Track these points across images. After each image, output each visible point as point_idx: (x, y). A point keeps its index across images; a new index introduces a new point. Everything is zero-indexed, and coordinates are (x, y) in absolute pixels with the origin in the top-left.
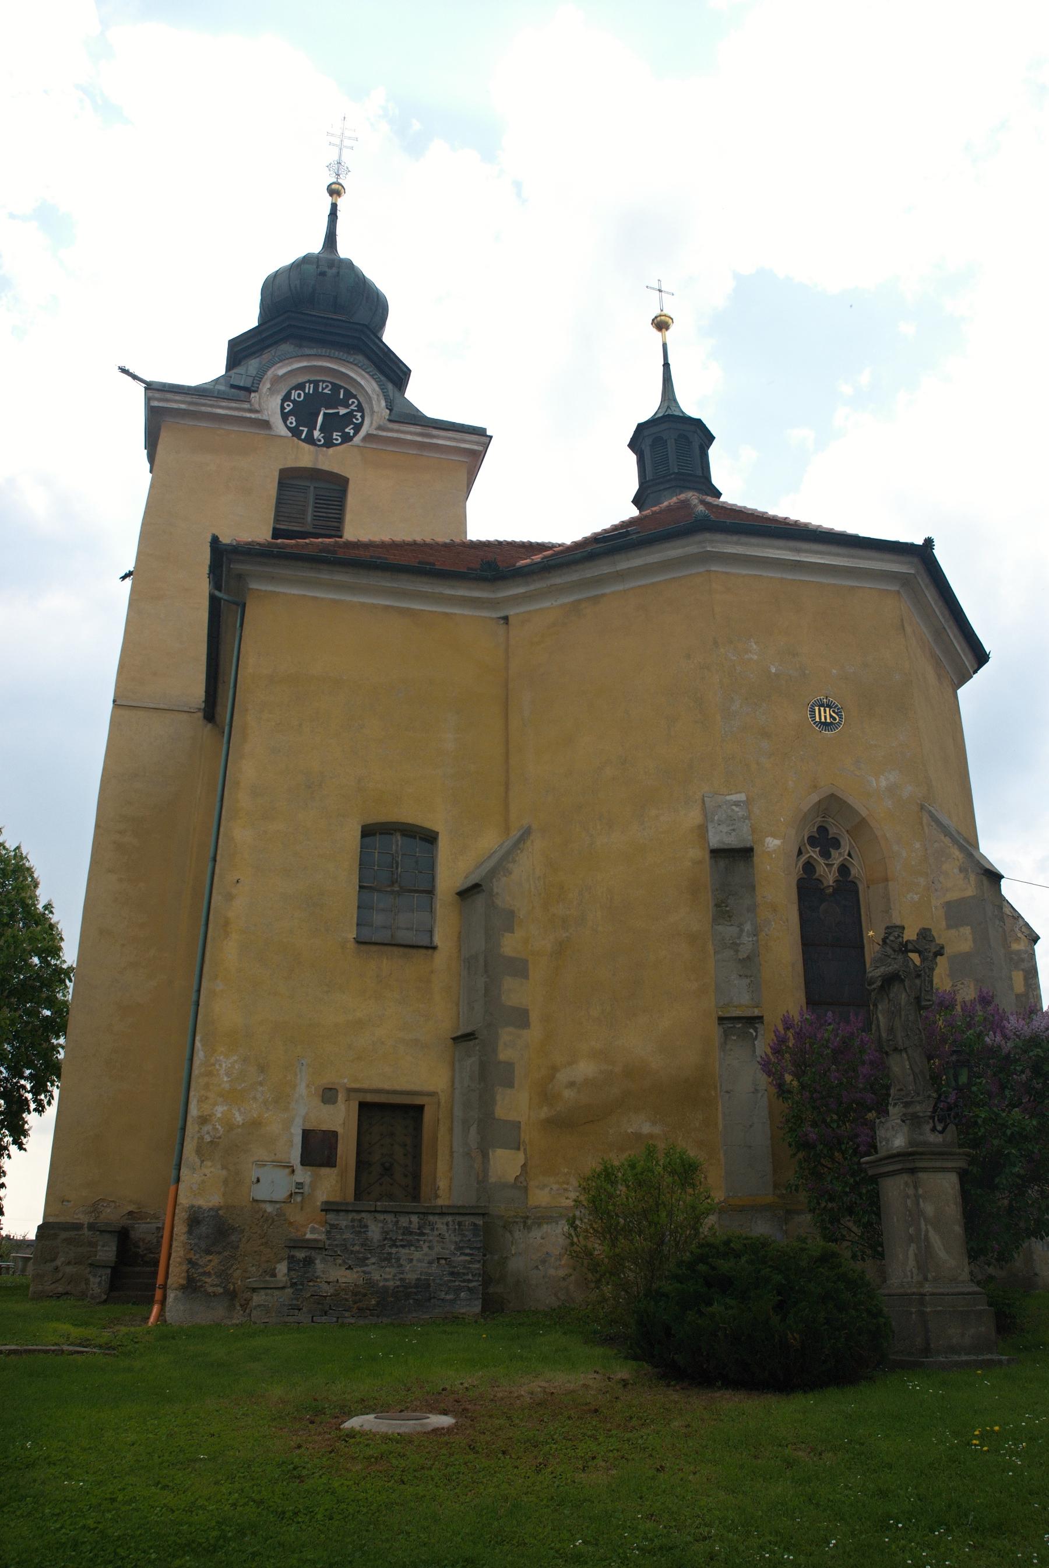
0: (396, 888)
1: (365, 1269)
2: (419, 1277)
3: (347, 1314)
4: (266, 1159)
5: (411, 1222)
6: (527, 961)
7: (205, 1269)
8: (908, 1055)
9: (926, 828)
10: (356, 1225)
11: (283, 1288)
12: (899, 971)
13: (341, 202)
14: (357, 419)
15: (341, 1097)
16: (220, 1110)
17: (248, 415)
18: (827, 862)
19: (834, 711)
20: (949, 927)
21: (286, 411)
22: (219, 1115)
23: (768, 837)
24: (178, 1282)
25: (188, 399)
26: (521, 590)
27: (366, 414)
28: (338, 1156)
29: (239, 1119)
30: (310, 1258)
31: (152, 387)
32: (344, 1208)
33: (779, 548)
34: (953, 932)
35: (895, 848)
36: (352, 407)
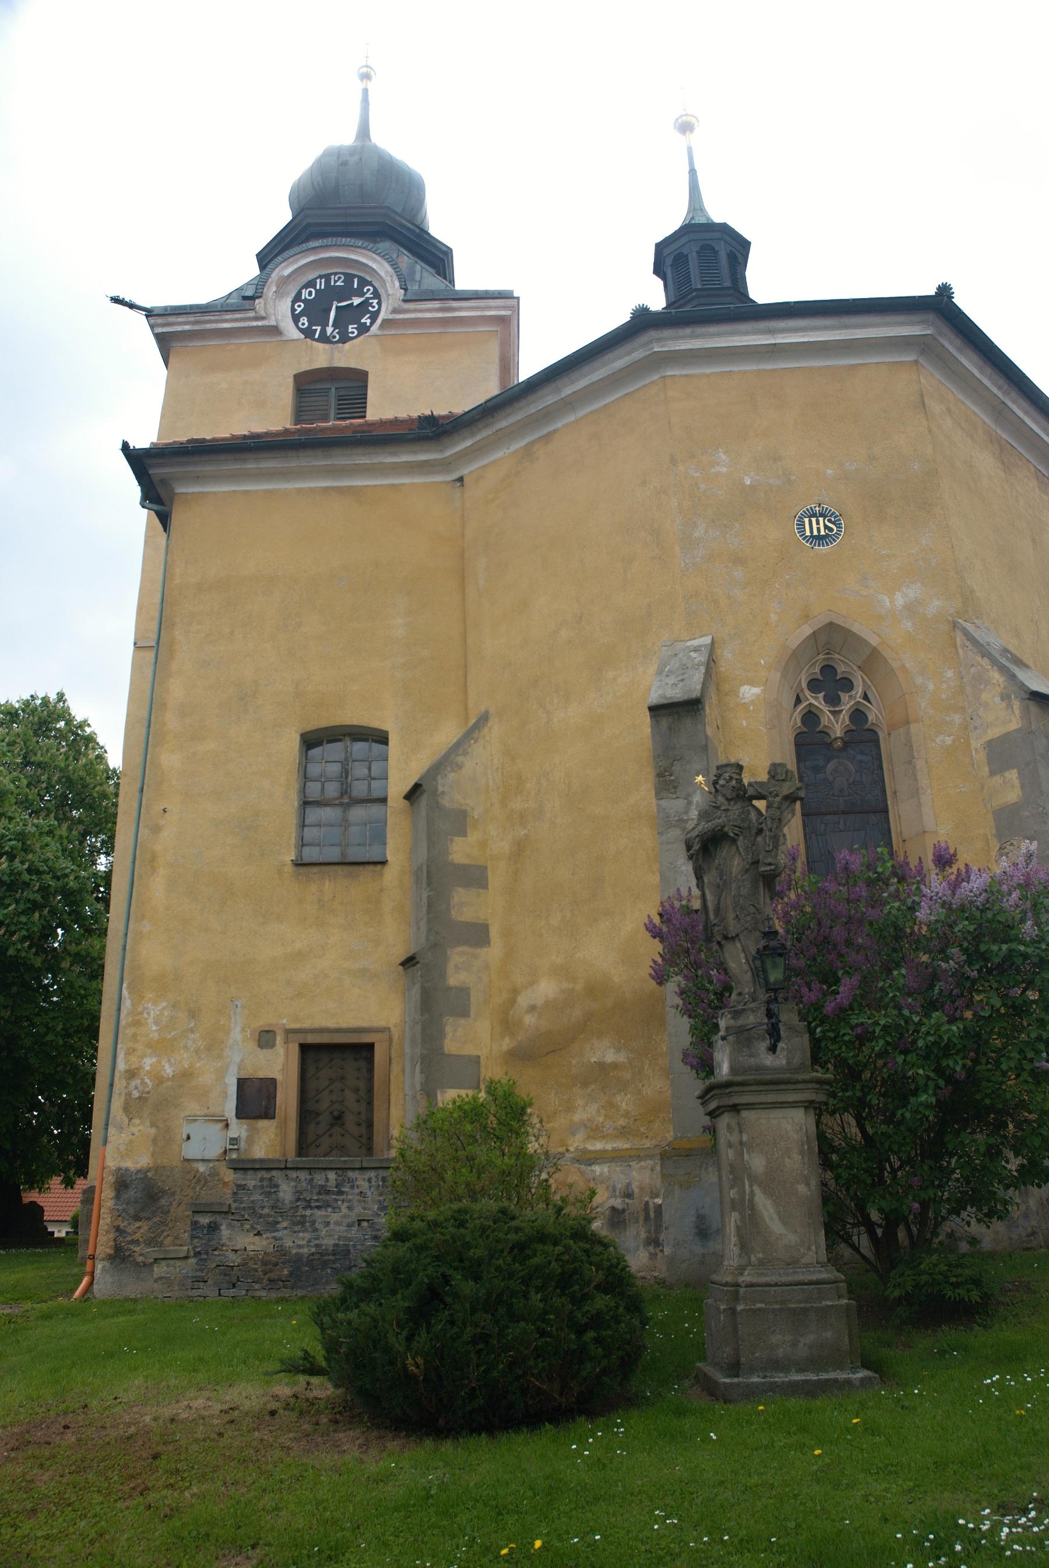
0: (346, 800)
1: (276, 1234)
2: (337, 1242)
3: (257, 1286)
4: (199, 1113)
5: (327, 1180)
6: (486, 868)
7: (134, 1237)
8: (741, 943)
9: (960, 651)
10: (265, 1184)
11: (186, 1258)
12: (723, 827)
13: (371, 86)
14: (374, 307)
15: (279, 1039)
16: (148, 1063)
17: (255, 324)
18: (832, 709)
19: (829, 521)
20: (992, 773)
21: (297, 312)
22: (147, 1068)
24: (105, 1252)
25: (191, 318)
26: (468, 443)
27: (383, 300)
28: (277, 1106)
29: (169, 1071)
30: (215, 1223)
31: (154, 313)
32: (250, 1166)
33: (746, 333)
34: (997, 779)
35: (919, 680)
36: (368, 295)
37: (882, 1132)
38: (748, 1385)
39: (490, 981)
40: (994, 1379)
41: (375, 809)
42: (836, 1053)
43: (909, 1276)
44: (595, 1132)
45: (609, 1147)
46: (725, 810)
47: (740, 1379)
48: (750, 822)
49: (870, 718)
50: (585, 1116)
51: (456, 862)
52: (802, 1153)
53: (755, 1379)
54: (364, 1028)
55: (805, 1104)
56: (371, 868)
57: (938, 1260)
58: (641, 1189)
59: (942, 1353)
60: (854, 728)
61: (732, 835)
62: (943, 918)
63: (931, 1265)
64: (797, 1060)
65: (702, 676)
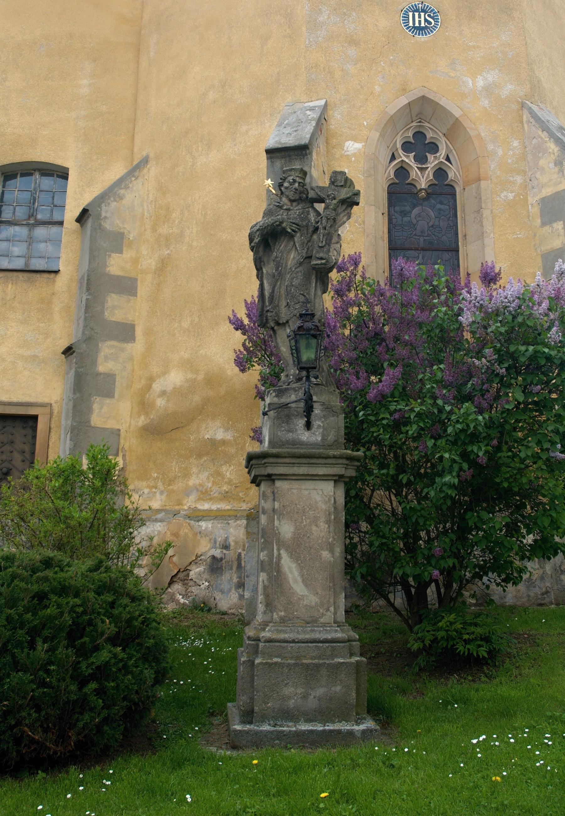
6: (136, 280)
9: (526, 126)
12: (281, 223)
19: (429, 16)
20: (544, 224)
23: (349, 140)
34: (547, 229)
35: (491, 147)
37: (411, 507)
38: (257, 733)
39: (133, 370)
40: (481, 739)
41: (54, 229)
42: (375, 434)
43: (428, 631)
44: (205, 495)
45: (214, 507)
46: (286, 209)
47: (252, 727)
48: (309, 221)
49: (450, 176)
50: (198, 482)
51: (112, 273)
52: (328, 522)
53: (266, 727)
54: (31, 403)
55: (335, 478)
56: (46, 275)
57: (455, 619)
58: (236, 543)
59: (446, 703)
60: (437, 183)
61: (289, 230)
62: (478, 319)
63: (448, 623)
64: (331, 438)
65: (313, 128)
